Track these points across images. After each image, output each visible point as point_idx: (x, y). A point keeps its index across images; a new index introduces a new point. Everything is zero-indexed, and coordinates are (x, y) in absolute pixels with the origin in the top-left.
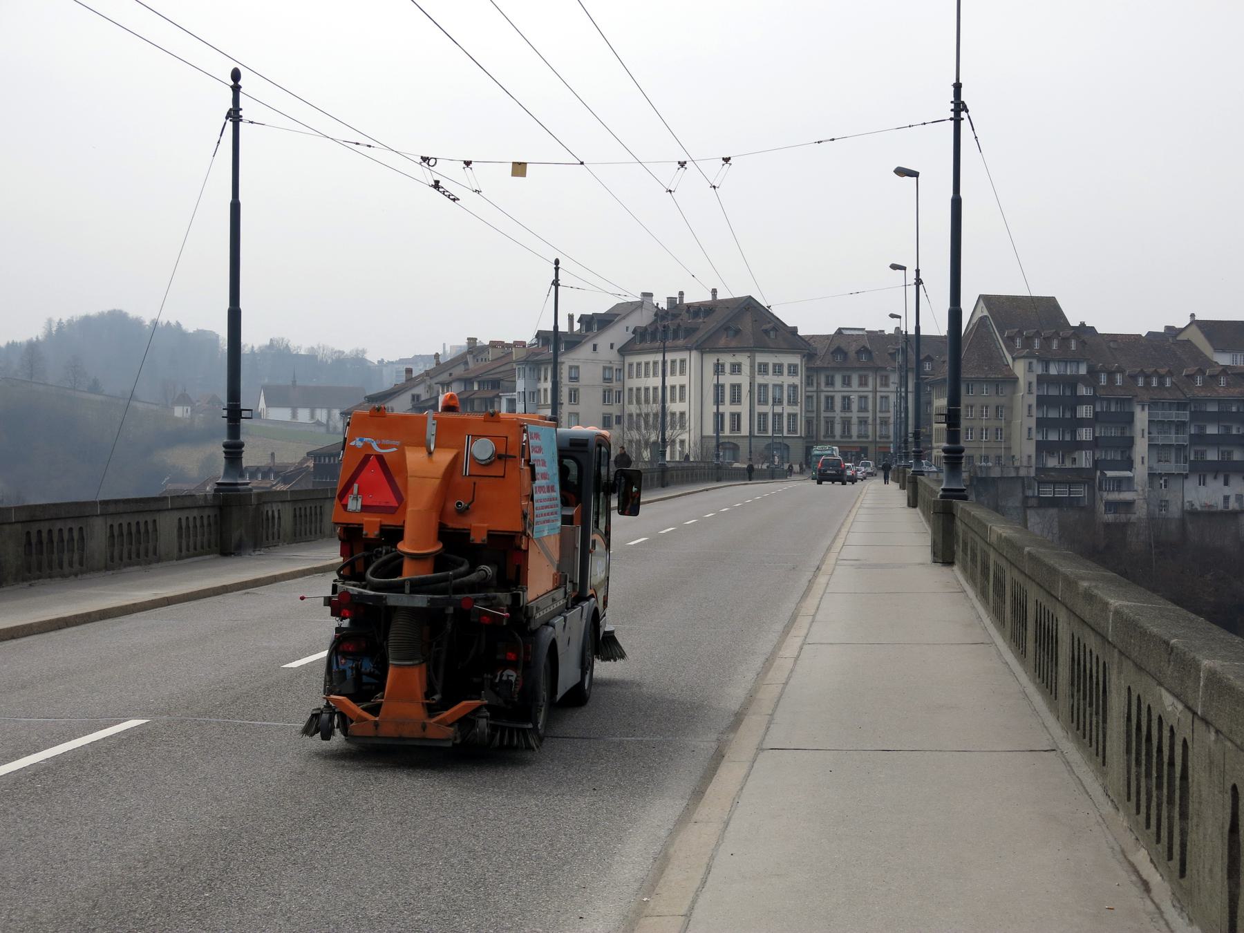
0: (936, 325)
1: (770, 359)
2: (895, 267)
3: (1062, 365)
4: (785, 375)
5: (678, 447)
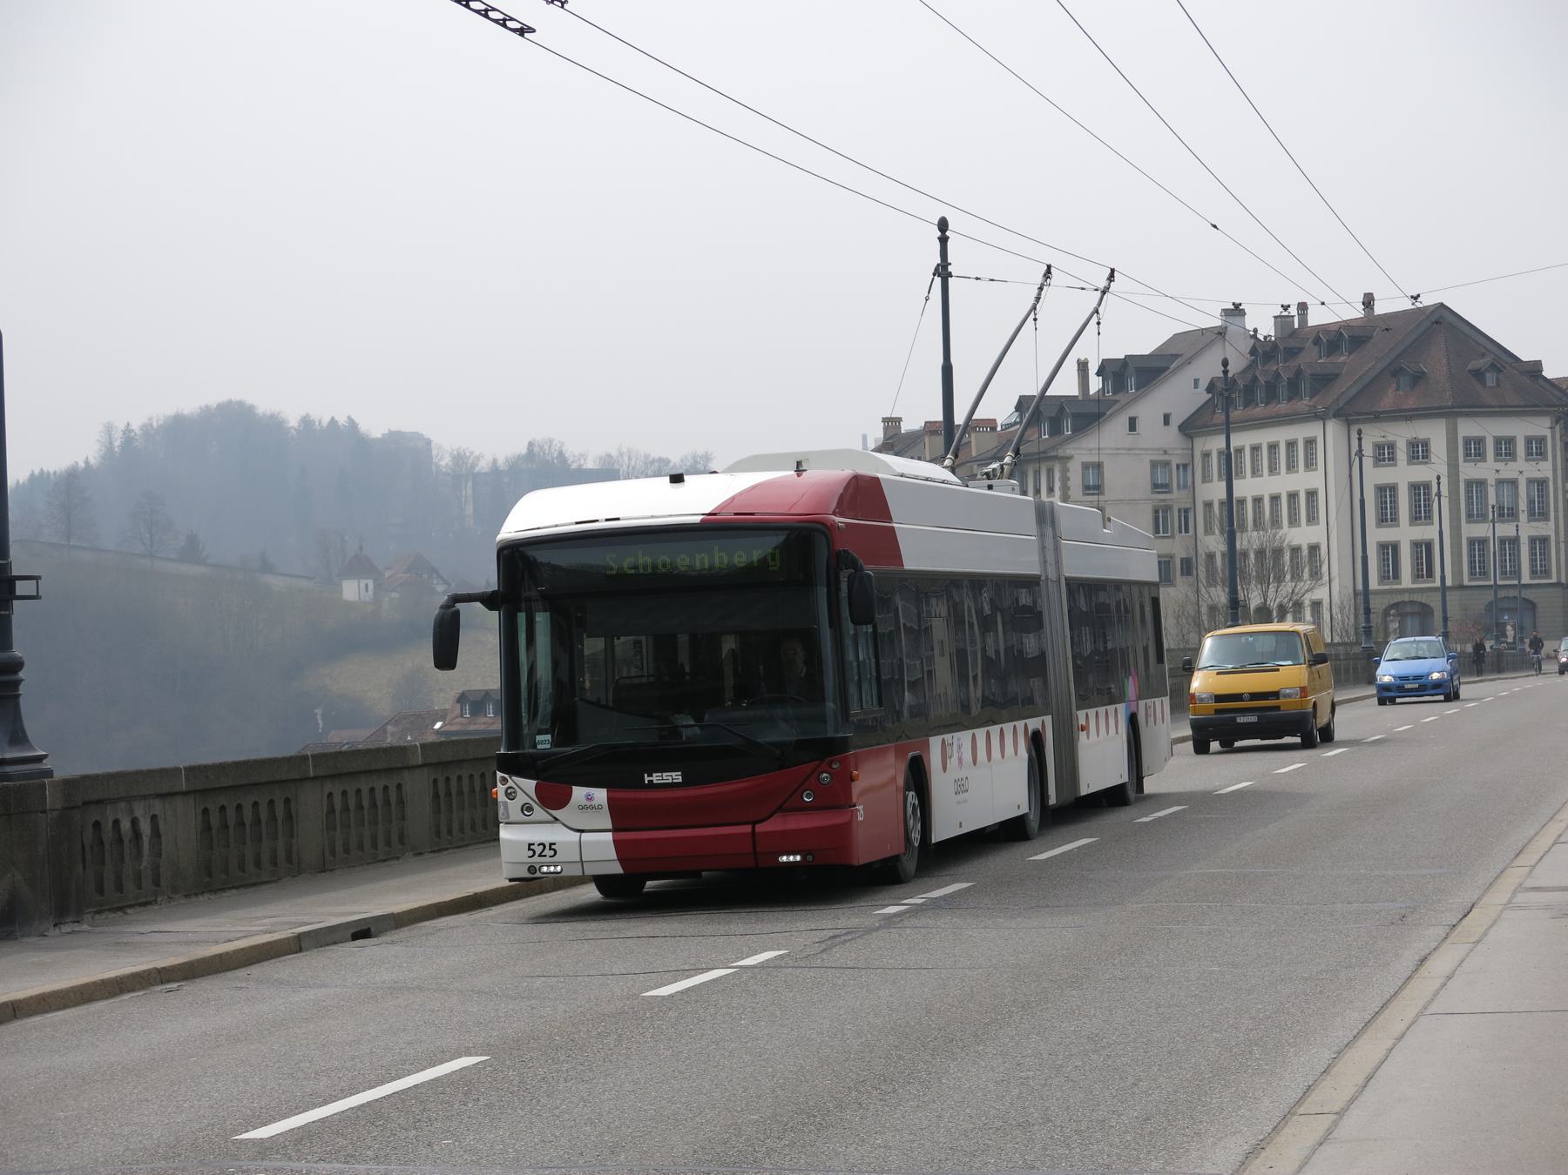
1: (1490, 429)
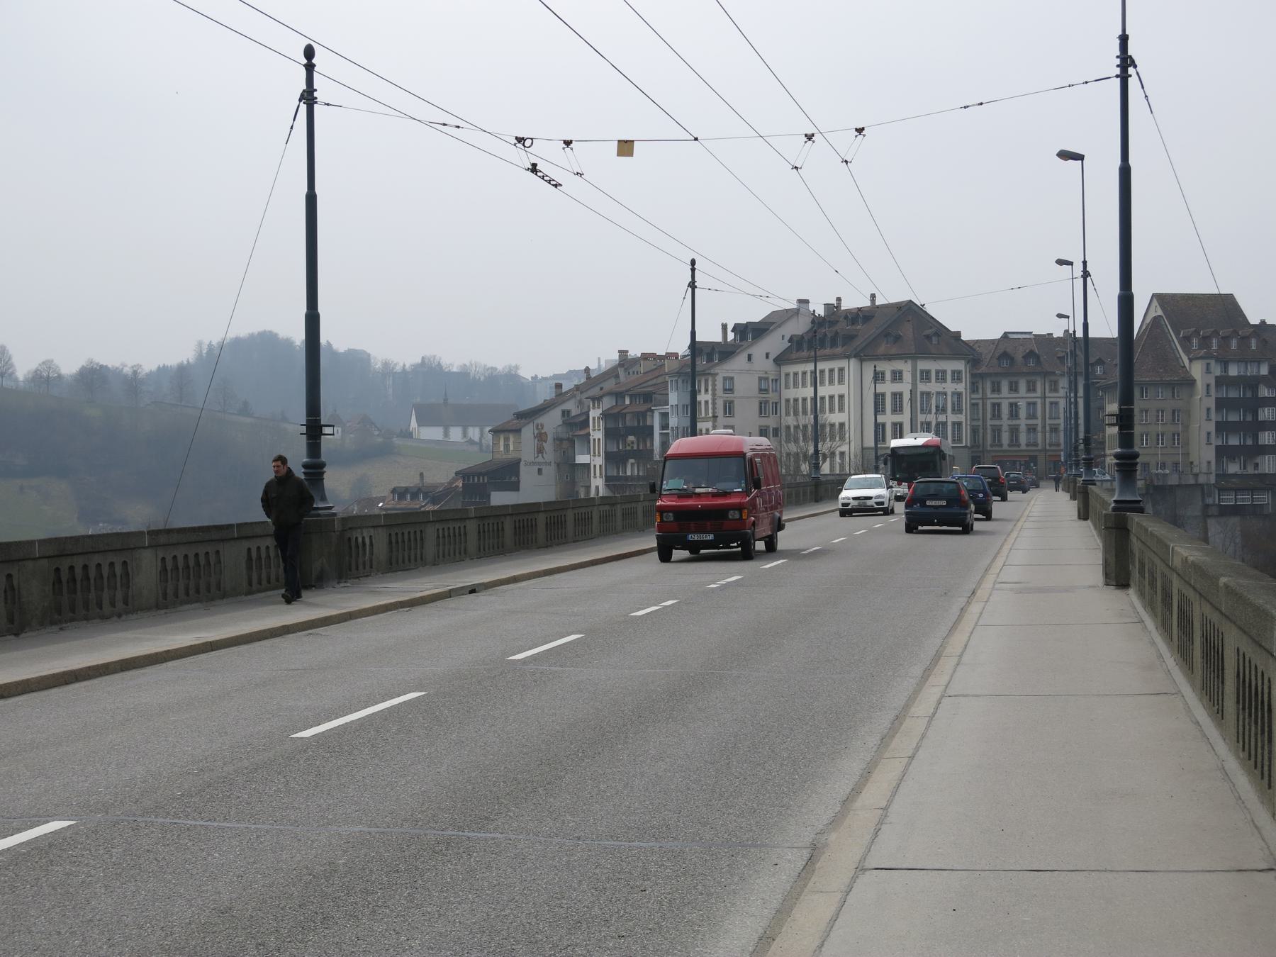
0: (1105, 326)
1: (932, 366)
2: (1061, 262)
3: (1242, 365)
4: (950, 380)
5: (838, 459)
